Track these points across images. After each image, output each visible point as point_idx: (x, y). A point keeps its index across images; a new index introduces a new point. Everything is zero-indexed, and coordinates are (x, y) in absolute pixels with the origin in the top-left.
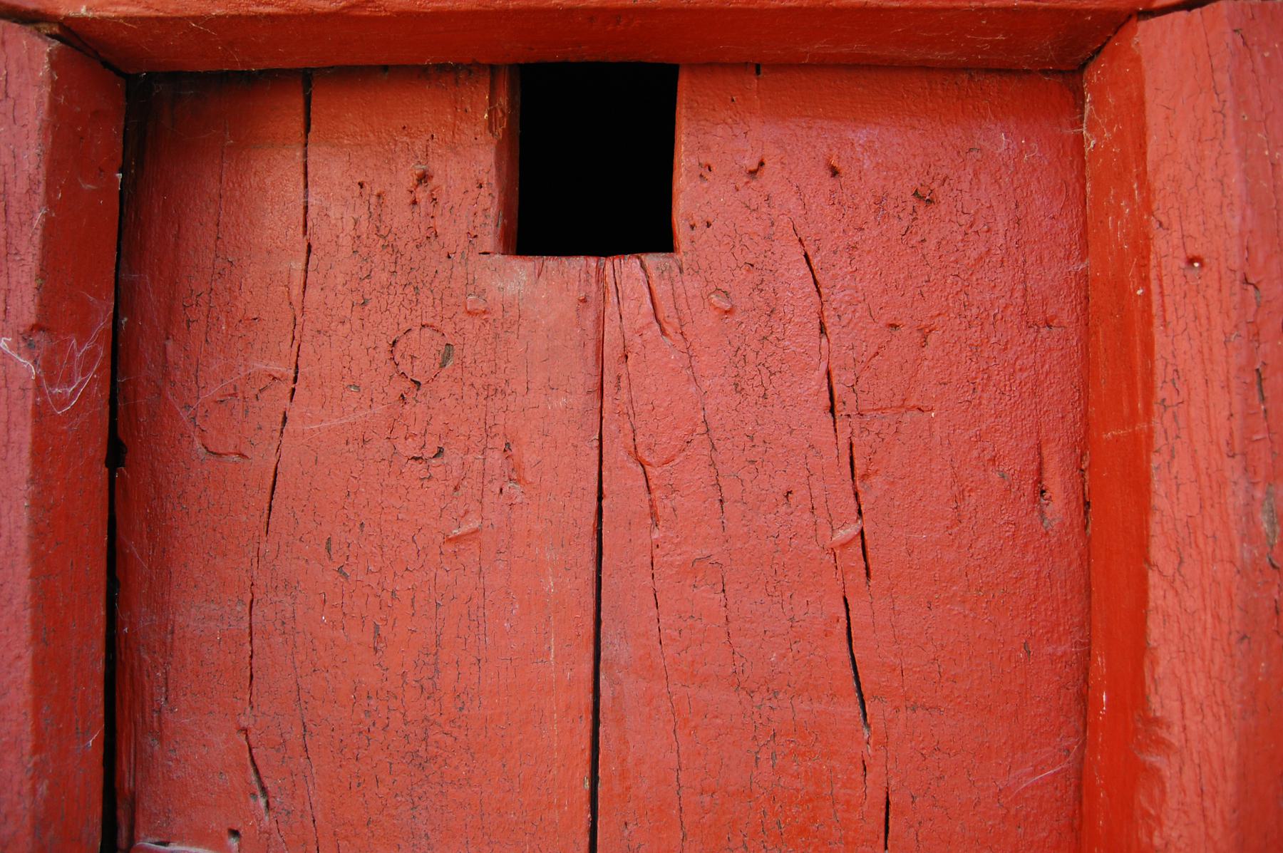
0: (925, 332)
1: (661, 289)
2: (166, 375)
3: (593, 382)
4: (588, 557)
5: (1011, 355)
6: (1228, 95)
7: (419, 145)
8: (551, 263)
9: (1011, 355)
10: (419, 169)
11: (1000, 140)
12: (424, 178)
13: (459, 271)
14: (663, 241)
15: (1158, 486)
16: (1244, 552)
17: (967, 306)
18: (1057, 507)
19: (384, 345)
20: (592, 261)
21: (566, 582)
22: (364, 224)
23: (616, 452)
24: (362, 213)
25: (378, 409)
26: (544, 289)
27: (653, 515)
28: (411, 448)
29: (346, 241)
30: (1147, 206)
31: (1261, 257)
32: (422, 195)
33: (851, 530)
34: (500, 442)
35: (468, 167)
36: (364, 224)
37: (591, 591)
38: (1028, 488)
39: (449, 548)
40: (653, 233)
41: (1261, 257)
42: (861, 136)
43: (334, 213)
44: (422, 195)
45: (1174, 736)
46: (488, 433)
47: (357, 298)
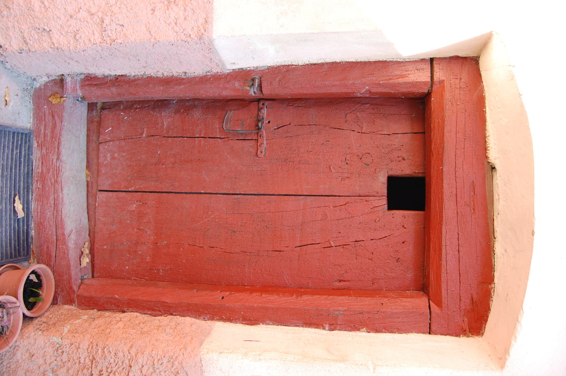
0: (371, 259)
1: (380, 208)
2: (363, 104)
3: (361, 194)
4: (327, 194)
5: (367, 276)
6: (411, 311)
7: (410, 158)
8: (386, 186)
9: (367, 276)
10: (406, 158)
11: (410, 275)
12: (404, 159)
13: (384, 167)
14: (390, 208)
15: (342, 297)
16: (331, 309)
17: (376, 268)
18: (337, 284)
19: (369, 152)
20: (386, 194)
21: (323, 189)
22: (394, 146)
23: (348, 199)
24: (397, 146)
25: (356, 151)
26: (380, 184)
27: (335, 207)
28: (348, 158)
29: (391, 143)
30: (393, 298)
31: (383, 314)
32: (400, 158)
33: (333, 245)
34: (349, 176)
35: (406, 168)
36: (394, 146)
37: (320, 194)
38: (341, 278)
39: (328, 166)
40: (392, 206)
41: (383, 314)
42: (411, 248)
43: (397, 140)
44: (400, 158)
45: (299, 299)
46: (351, 173)
47: (379, 146)
